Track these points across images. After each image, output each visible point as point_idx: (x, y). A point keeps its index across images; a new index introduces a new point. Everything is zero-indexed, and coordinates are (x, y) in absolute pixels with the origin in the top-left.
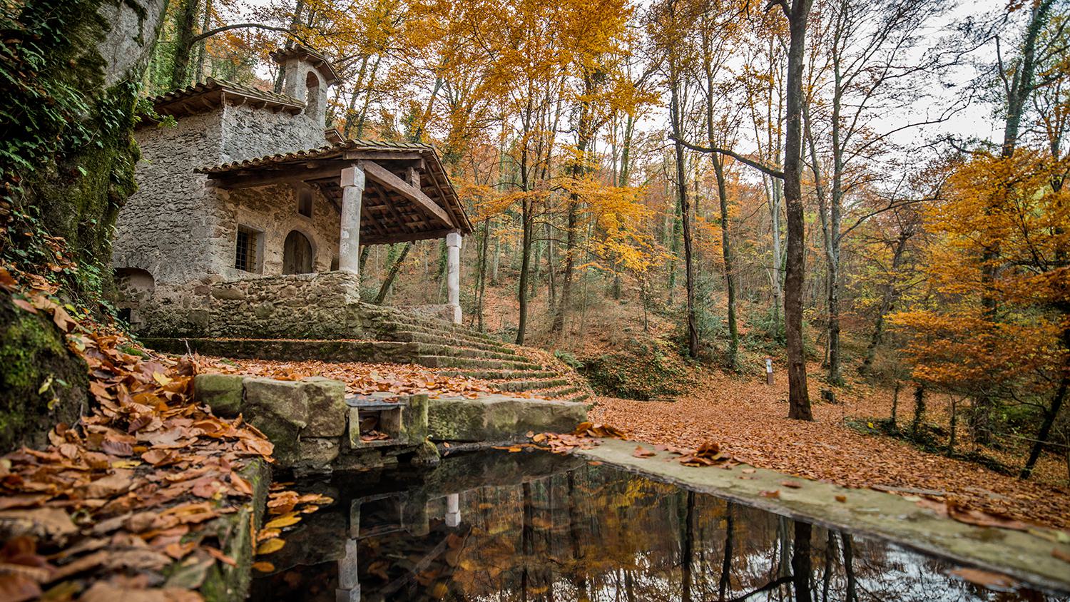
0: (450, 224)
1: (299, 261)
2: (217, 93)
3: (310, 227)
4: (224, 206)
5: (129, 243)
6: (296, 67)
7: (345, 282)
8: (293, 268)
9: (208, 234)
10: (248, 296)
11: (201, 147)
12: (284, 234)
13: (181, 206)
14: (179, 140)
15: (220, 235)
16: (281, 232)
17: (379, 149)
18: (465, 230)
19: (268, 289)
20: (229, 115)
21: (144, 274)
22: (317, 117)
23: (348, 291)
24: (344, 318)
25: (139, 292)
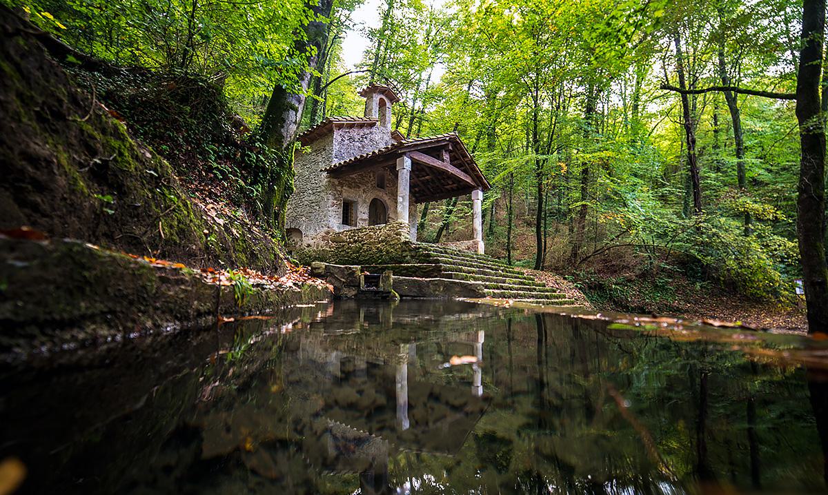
4: (336, 189)
12: (369, 201)
13: (314, 191)
18: (485, 189)
23: (403, 234)
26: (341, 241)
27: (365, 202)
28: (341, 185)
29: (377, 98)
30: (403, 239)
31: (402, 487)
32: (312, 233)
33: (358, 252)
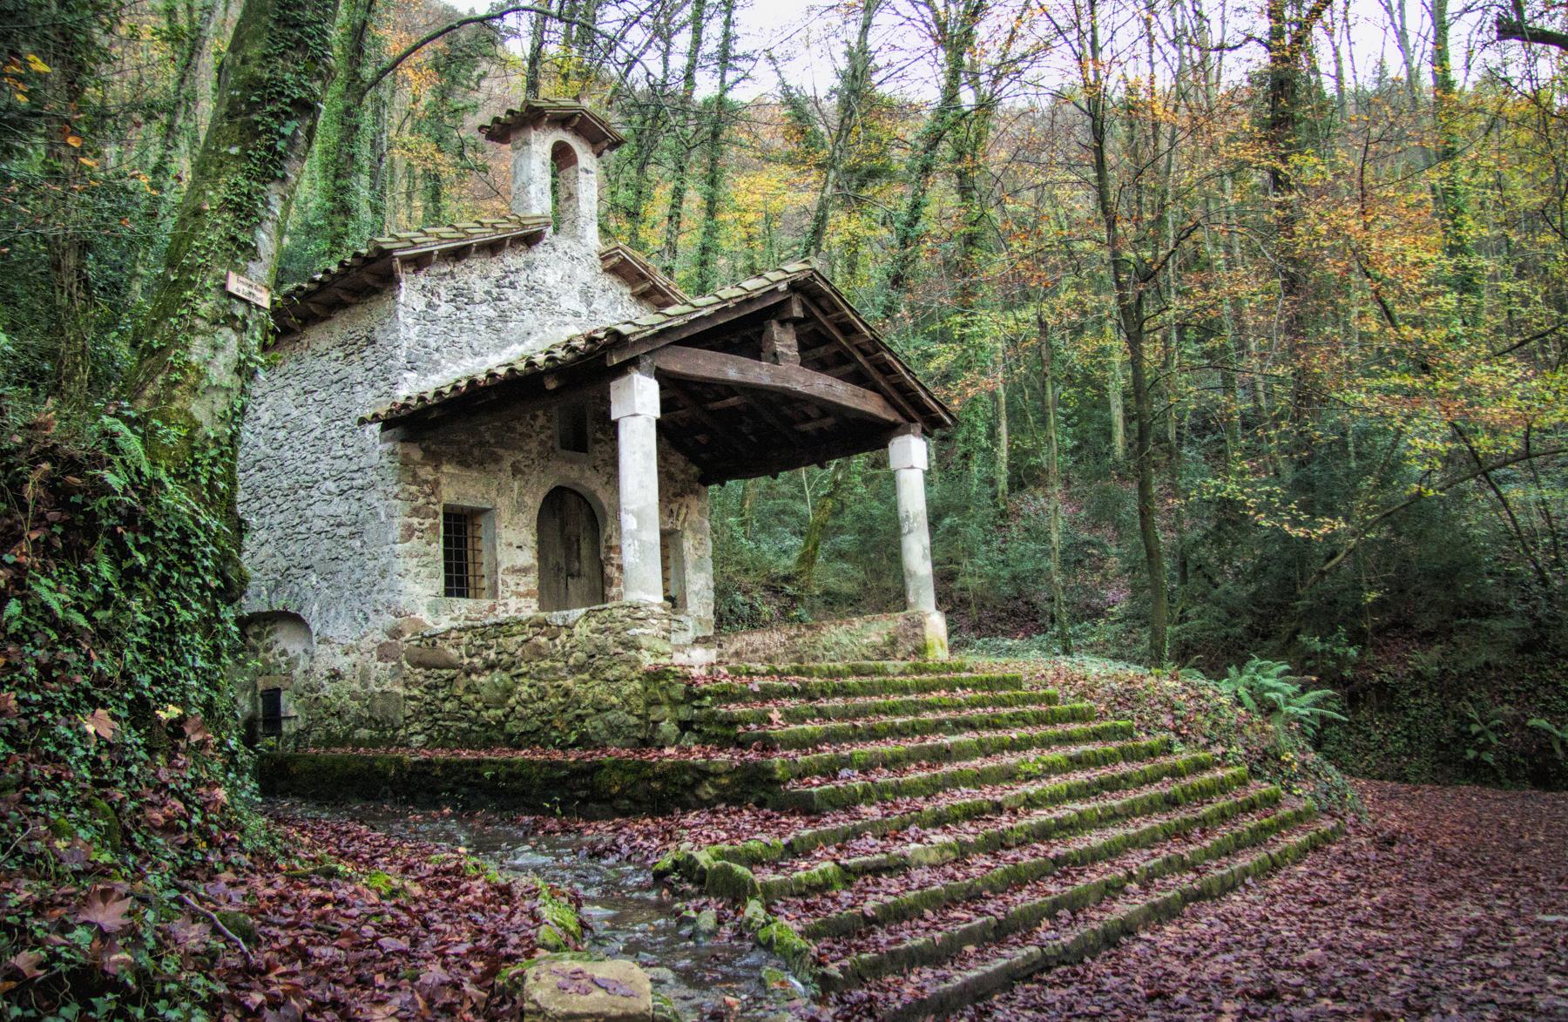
0: (891, 416)
1: (570, 547)
2: (386, 260)
3: (588, 473)
4: (415, 475)
5: (269, 564)
6: (527, 143)
7: (635, 626)
8: (560, 570)
9: (390, 538)
10: (466, 661)
11: (369, 365)
12: (534, 502)
13: (344, 484)
14: (334, 355)
15: (411, 536)
16: (528, 500)
17: (680, 321)
18: (931, 422)
19: (499, 645)
20: (410, 293)
21: (295, 620)
22: (579, 233)
23: (644, 642)
24: (641, 702)
25: (291, 655)
26: (441, 661)
27: (520, 507)
28: (434, 458)
29: (541, 144)
30: (647, 661)
31: (1242, 458)
32: (341, 630)
33: (500, 704)
